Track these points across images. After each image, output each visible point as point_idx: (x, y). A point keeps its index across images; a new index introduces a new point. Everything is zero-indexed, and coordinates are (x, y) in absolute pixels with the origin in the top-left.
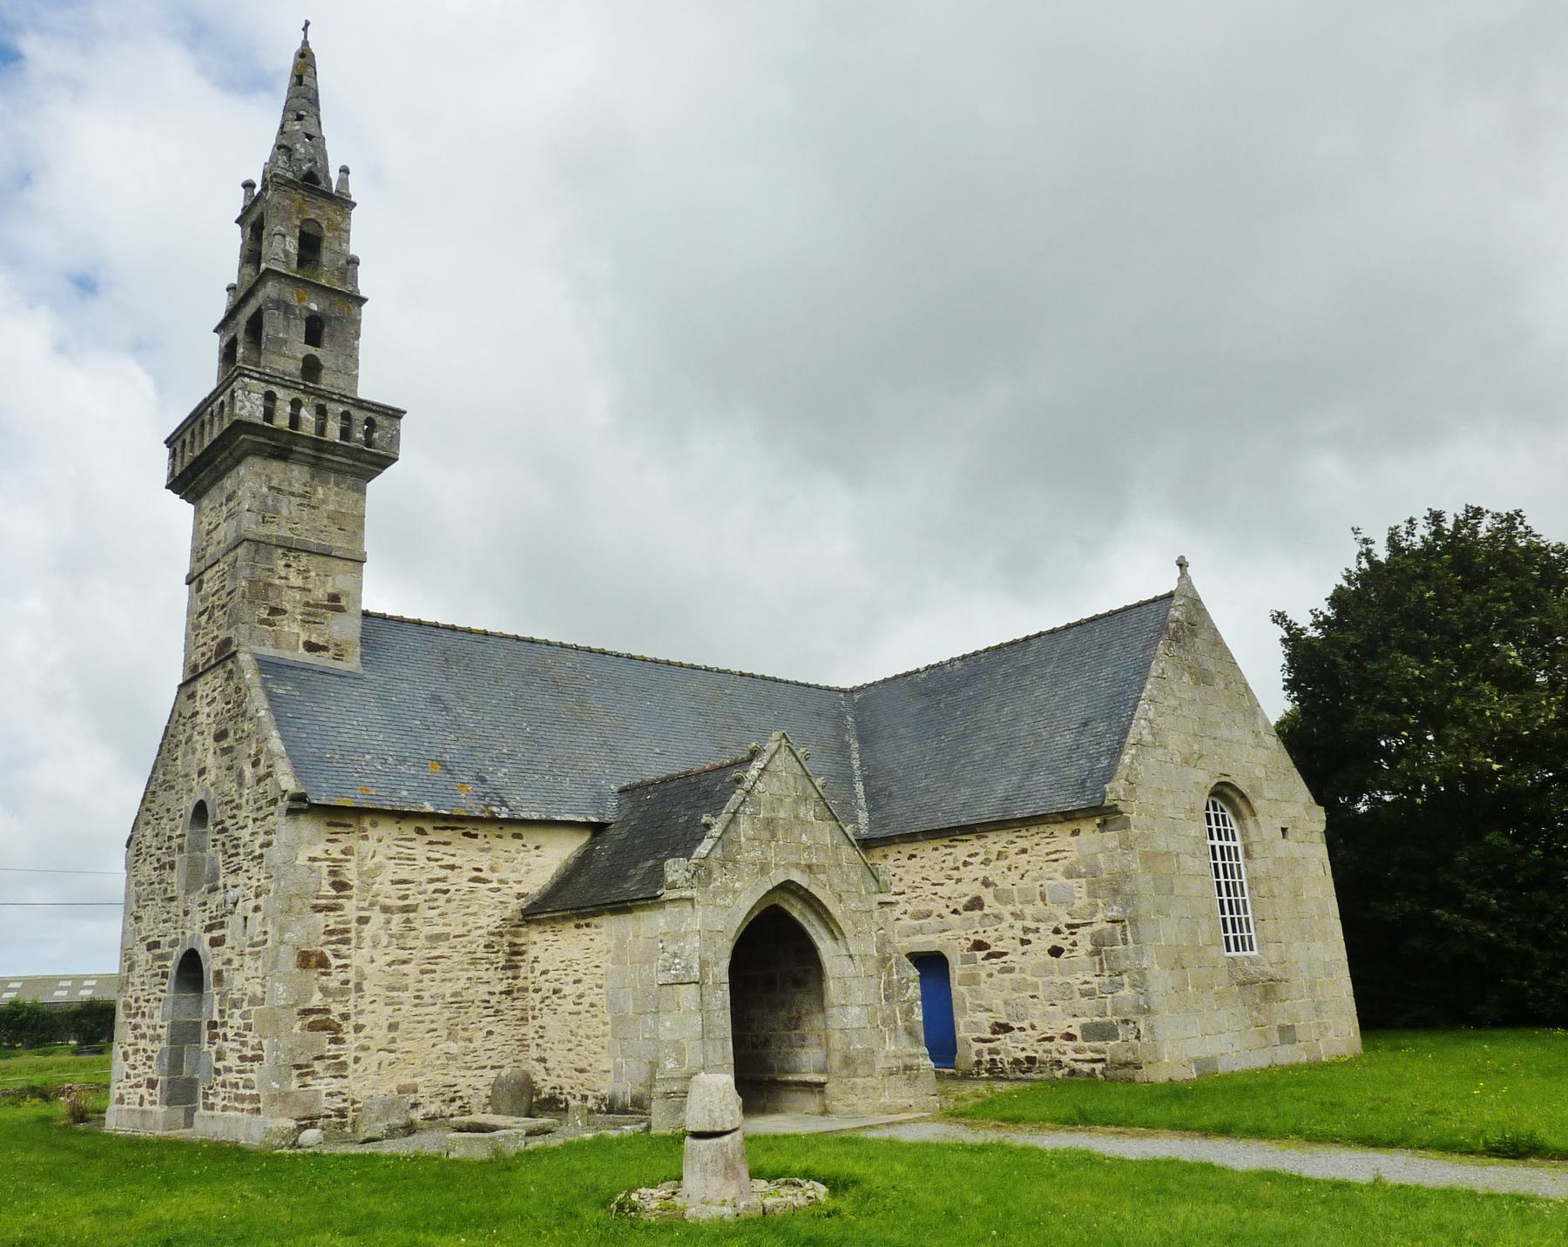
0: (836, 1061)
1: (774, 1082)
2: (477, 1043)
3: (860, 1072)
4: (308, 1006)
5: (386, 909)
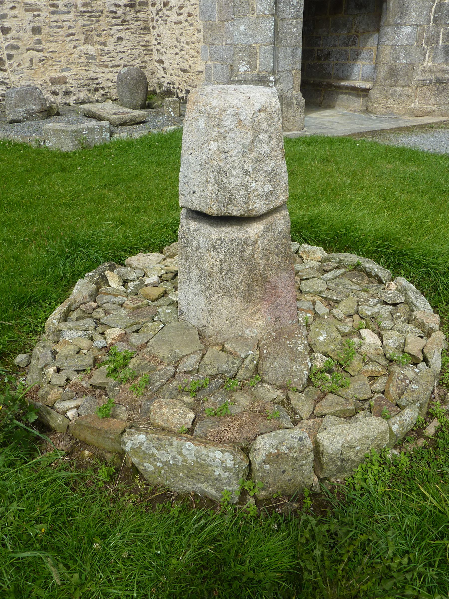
0: (383, 72)
1: (330, 86)
2: (110, 47)
3: (400, 82)
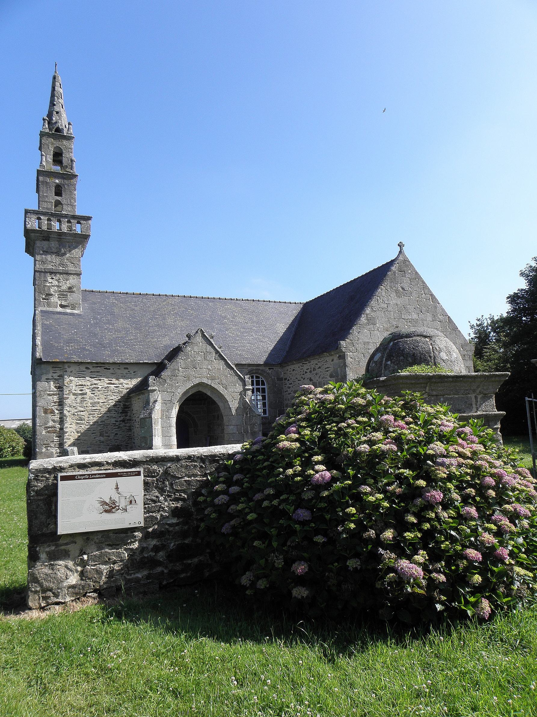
4: (47, 426)
5: (74, 394)
